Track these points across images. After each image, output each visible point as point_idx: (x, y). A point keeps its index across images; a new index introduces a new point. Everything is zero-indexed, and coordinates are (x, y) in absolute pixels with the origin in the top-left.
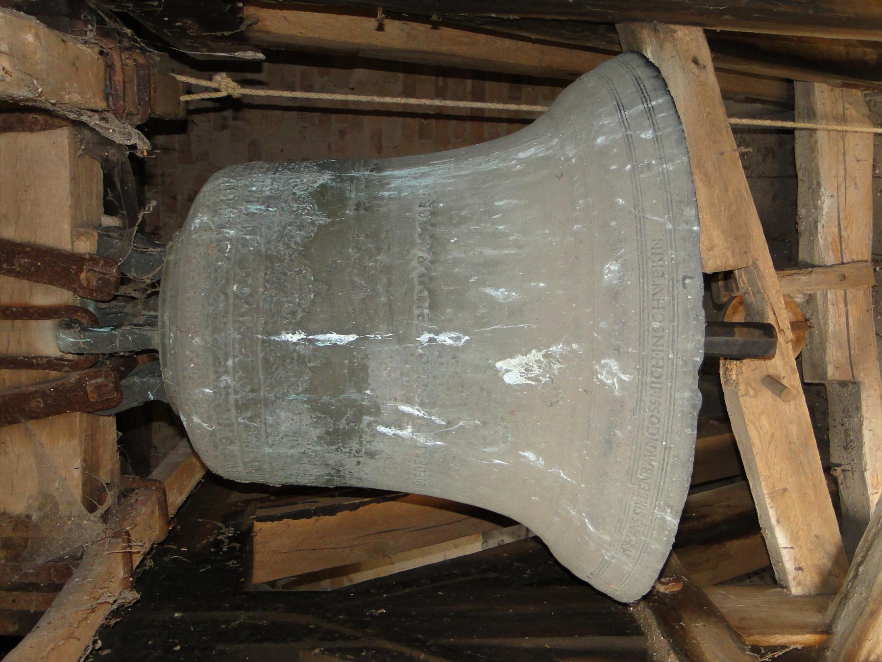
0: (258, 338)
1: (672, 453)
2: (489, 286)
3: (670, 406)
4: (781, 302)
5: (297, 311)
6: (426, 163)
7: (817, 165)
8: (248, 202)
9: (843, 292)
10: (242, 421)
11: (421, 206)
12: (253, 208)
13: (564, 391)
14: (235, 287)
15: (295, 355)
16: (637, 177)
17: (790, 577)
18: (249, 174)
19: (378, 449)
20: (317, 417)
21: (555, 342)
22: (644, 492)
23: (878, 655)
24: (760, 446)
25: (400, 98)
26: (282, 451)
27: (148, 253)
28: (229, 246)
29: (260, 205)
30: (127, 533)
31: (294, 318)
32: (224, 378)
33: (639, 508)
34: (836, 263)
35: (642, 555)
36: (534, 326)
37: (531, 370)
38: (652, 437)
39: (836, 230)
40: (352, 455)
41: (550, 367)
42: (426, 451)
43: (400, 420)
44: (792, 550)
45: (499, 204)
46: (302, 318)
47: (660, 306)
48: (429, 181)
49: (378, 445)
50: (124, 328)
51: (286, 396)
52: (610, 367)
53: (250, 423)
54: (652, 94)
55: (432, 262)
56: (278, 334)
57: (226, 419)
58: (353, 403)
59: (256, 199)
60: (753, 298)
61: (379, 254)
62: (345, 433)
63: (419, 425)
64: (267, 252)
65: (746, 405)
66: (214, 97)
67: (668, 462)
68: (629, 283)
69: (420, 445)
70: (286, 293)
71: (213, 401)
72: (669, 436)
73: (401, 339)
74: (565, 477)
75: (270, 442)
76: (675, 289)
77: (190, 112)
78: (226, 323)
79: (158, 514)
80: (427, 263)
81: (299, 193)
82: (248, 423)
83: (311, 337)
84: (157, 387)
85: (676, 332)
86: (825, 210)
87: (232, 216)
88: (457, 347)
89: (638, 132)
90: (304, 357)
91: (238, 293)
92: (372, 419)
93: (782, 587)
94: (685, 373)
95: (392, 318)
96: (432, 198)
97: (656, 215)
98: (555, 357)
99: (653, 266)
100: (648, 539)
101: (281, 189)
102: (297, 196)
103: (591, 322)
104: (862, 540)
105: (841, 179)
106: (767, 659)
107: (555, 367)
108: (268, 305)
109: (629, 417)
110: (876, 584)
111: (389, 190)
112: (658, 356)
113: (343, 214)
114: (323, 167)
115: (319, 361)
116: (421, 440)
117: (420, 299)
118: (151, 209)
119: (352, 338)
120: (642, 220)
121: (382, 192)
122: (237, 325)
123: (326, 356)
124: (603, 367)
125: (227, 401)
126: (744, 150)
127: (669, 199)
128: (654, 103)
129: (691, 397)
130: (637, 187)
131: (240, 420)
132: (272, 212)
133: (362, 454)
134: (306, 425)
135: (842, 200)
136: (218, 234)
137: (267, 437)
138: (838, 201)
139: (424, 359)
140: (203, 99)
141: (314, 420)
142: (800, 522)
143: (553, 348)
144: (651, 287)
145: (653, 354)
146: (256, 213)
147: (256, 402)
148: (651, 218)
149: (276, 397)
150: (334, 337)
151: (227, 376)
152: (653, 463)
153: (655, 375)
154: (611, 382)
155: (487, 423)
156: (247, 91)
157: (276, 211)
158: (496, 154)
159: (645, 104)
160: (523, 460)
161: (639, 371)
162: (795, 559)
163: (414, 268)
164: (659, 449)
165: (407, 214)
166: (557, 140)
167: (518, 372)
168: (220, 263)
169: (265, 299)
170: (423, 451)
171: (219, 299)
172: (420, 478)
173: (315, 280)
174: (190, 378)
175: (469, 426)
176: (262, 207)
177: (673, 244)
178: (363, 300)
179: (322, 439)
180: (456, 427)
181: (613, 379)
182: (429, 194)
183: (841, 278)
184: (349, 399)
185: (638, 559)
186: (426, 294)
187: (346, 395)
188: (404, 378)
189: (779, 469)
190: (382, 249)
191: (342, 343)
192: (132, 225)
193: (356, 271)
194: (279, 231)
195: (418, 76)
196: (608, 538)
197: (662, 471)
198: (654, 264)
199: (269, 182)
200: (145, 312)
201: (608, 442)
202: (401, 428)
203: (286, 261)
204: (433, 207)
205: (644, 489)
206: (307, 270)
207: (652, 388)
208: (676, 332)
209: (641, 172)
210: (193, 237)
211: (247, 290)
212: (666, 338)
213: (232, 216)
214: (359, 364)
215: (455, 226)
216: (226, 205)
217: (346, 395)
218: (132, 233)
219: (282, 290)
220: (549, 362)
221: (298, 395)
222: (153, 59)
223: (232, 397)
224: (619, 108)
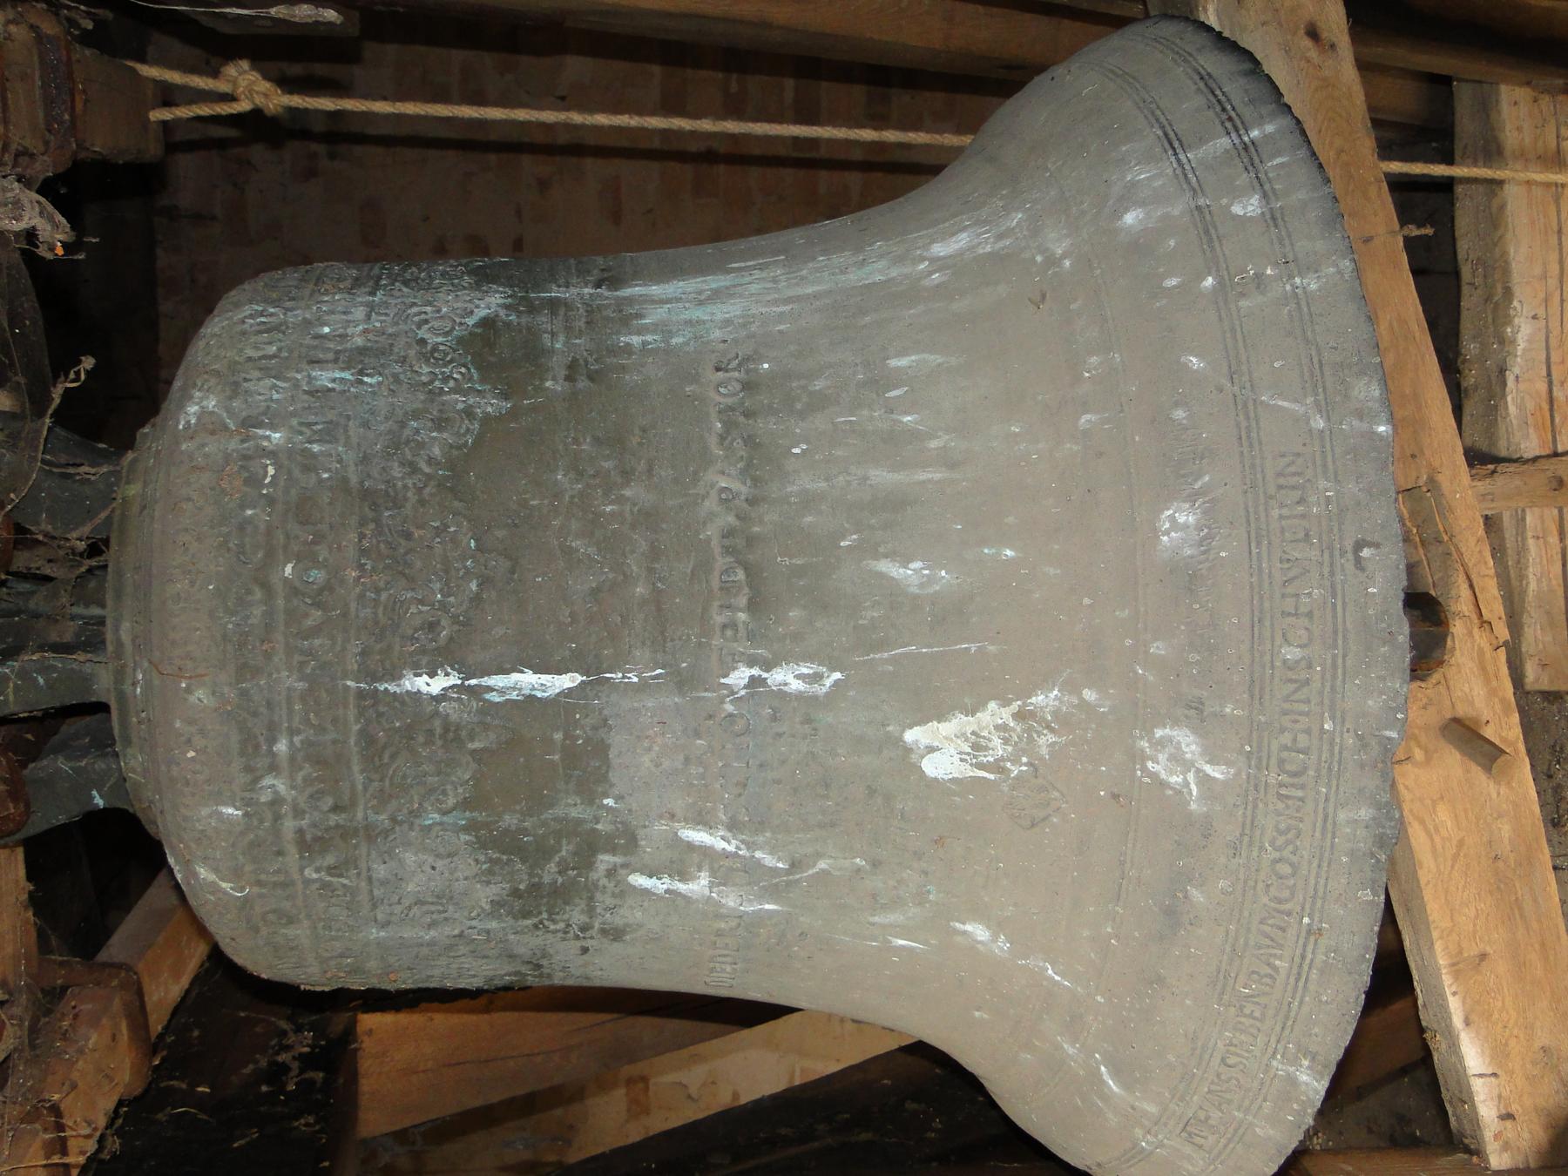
0: (347, 688)
1: (1323, 941)
2: (886, 556)
4: (1486, 563)
5: (438, 622)
6: (719, 267)
7: (1505, 253)
8: (314, 362)
9: (1556, 512)
10: (315, 876)
11: (718, 369)
12: (325, 377)
14: (289, 569)
15: (437, 723)
16: (1233, 306)
17: (1488, 1135)
18: (311, 295)
19: (631, 922)
20: (491, 860)
21: (1044, 684)
22: (1252, 1021)
24: (1433, 866)
25: (627, 116)
26: (408, 933)
27: (78, 478)
28: (271, 471)
29: (343, 369)
30: (55, 1110)
31: (432, 640)
32: (268, 781)
33: (1238, 1055)
34: (1543, 454)
35: (1231, 1146)
36: (992, 648)
37: (986, 748)
38: (1278, 906)
39: (1542, 386)
40: (571, 935)
41: (1031, 740)
42: (739, 924)
43: (683, 861)
44: (1493, 1079)
45: (899, 364)
46: (451, 639)
47: (1303, 610)
48: (731, 309)
49: (630, 914)
50: (26, 658)
51: (416, 817)
52: (1178, 746)
53: (334, 880)
54: (1247, 112)
55: (752, 502)
56: (395, 676)
57: (278, 871)
58: (571, 828)
59: (330, 356)
60: (1421, 551)
61: (627, 483)
62: (555, 892)
63: (723, 868)
64: (361, 483)
65: (1406, 783)
66: (224, 113)
67: (1312, 960)
69: (725, 911)
70: (411, 580)
71: (242, 833)
73: (683, 682)
74: (1057, 978)
75: (380, 916)
76: (1338, 570)
77: (172, 147)
78: (268, 656)
79: (126, 1038)
80: (740, 503)
81: (433, 339)
82: (328, 878)
83: (473, 682)
84: (113, 780)
85: (1340, 671)
86: (1522, 344)
87: (276, 396)
88: (815, 698)
89: (1224, 201)
90: (458, 727)
91: (297, 584)
92: (618, 860)
93: (1468, 1150)
94: (1362, 766)
95: (662, 633)
96: (745, 349)
97: (1281, 396)
98: (1044, 719)
99: (1281, 517)
100: (1250, 1118)
101: (390, 331)
102: (429, 348)
103: (1128, 642)
105: (1553, 282)
107: (1042, 741)
108: (368, 610)
109: (1223, 860)
111: (640, 331)
112: (1297, 726)
113: (539, 390)
114: (484, 278)
115: (492, 736)
116: (731, 901)
117: (726, 588)
118: (83, 377)
119: (569, 681)
120: (1251, 407)
121: (625, 335)
122: (297, 658)
123: (510, 725)
124: (1161, 744)
125: (276, 832)
126: (1415, 232)
127: (1315, 360)
128: (1255, 133)
129: (1374, 819)
130: (1233, 330)
131: (310, 873)
132: (371, 385)
133: (594, 932)
134: (466, 879)
135: (1554, 323)
136: (243, 441)
137: (374, 906)
138: (1547, 327)
139: (739, 726)
140: (199, 119)
141: (484, 867)
142: (1512, 1021)
143: (1038, 699)
144: (1279, 565)
145: (1286, 721)
146: (333, 390)
147: (346, 833)
149: (393, 820)
150: (527, 680)
151: (275, 777)
152: (1277, 963)
153: (1288, 767)
155: (880, 863)
156: (297, 101)
157: (379, 383)
158: (880, 247)
159: (1234, 135)
160: (959, 939)
161: (1249, 758)
162: (1500, 1097)
163: (711, 516)
164: (1292, 932)
165: (687, 389)
166: (1020, 216)
167: (953, 752)
168: (249, 512)
169: (362, 596)
170: (733, 924)
171: (250, 598)
172: (724, 975)
173: (478, 548)
174: (187, 783)
175: (840, 869)
176: (347, 375)
177: (1330, 464)
178: (595, 592)
179: (502, 906)
180: (810, 872)
181: (1184, 773)
182: (735, 341)
183: (1555, 484)
184: (564, 819)
185: (1220, 1153)
186: (741, 575)
187: (559, 811)
188: (693, 770)
189: (1473, 913)
190: (633, 470)
191: (546, 695)
192: (40, 414)
193: (575, 525)
194: (390, 432)
195: (689, 72)
196: (1152, 1109)
197: (1297, 980)
198: (1285, 512)
199: (359, 313)
200: (77, 610)
201: (1171, 914)
202: (684, 877)
203: (409, 505)
204: (748, 372)
205: (1251, 1016)
206: (459, 525)
207: (1280, 797)
208: (1340, 671)
209: (1242, 295)
210: (184, 447)
211: (317, 575)
212: (1316, 685)
213: (276, 396)
214: (588, 740)
215: (802, 415)
216: (261, 369)
217: (559, 811)
218: (39, 431)
219: (402, 574)
220: (1029, 730)
221: (445, 813)
222: (78, 26)
223: (289, 825)
224: (1171, 144)
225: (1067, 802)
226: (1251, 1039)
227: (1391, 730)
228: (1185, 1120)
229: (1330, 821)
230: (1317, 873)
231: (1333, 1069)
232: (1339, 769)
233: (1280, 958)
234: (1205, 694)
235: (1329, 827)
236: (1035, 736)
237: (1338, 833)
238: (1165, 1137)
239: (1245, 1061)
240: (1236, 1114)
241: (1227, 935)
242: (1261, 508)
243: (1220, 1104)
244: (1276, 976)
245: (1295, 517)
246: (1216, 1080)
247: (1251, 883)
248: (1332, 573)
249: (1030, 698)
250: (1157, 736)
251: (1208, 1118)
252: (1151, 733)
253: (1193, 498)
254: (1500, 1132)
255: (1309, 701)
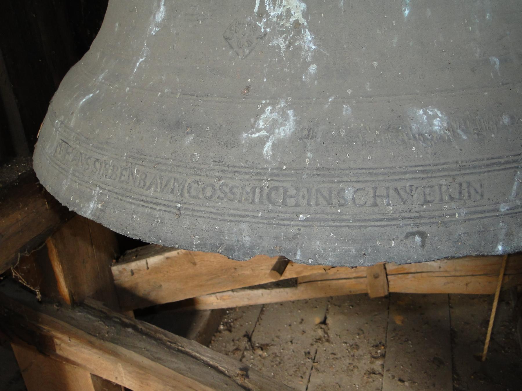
3: (229, 215)
9: (365, 275)
13: (246, 56)
17: (124, 266)
21: (319, 39)
22: (119, 175)
23: (60, 345)
35: (57, 167)
41: (281, 33)
44: (146, 268)
47: (379, 200)
52: (282, 125)
67: (155, 209)
68: (414, 149)
72: (188, 213)
74: (138, 64)
85: (338, 224)
94: (276, 238)
98: (295, 41)
99: (441, 185)
100: (70, 176)
104: (157, 327)
106: (14, 274)
107: (281, 40)
109: (212, 155)
110: (116, 346)
112: (301, 198)
124: (283, 114)
129: (243, 245)
135: (437, 274)
143: (309, 36)
144: (408, 185)
148: (516, 178)
154: (261, 126)
160: (155, 4)
162: (140, 270)
164: (172, 197)
181: (265, 129)
197: (143, 201)
198: (444, 188)
201: (178, 125)
205: (122, 174)
207: (254, 189)
208: (338, 224)
220: (288, 32)
225: (242, 59)
226: (110, 175)
227: (301, 255)
228: (67, 141)
229: (241, 219)
230: (207, 212)
231: (98, 221)
232: (274, 224)
233: (155, 191)
234: (319, 140)
235: (237, 219)
236: (284, 36)
237: (233, 223)
238: (60, 132)
239: (97, 173)
240: (72, 169)
241: (166, 159)
242: (446, 173)
243: (75, 160)
244: (145, 188)
245: (441, 194)
246: (87, 157)
247: (198, 172)
248: (403, 219)
249: (309, 31)
250: (289, 112)
251: (68, 153)
252: (291, 107)
253: (451, 129)
254: (126, 270)
255: (317, 205)
